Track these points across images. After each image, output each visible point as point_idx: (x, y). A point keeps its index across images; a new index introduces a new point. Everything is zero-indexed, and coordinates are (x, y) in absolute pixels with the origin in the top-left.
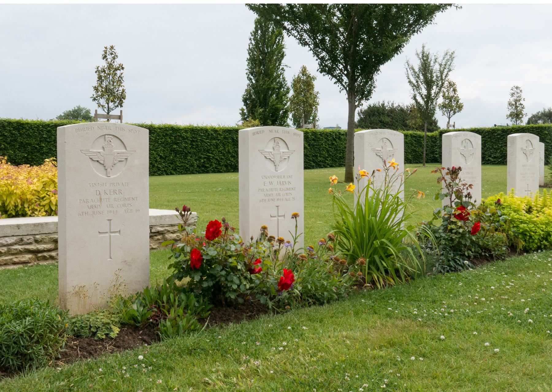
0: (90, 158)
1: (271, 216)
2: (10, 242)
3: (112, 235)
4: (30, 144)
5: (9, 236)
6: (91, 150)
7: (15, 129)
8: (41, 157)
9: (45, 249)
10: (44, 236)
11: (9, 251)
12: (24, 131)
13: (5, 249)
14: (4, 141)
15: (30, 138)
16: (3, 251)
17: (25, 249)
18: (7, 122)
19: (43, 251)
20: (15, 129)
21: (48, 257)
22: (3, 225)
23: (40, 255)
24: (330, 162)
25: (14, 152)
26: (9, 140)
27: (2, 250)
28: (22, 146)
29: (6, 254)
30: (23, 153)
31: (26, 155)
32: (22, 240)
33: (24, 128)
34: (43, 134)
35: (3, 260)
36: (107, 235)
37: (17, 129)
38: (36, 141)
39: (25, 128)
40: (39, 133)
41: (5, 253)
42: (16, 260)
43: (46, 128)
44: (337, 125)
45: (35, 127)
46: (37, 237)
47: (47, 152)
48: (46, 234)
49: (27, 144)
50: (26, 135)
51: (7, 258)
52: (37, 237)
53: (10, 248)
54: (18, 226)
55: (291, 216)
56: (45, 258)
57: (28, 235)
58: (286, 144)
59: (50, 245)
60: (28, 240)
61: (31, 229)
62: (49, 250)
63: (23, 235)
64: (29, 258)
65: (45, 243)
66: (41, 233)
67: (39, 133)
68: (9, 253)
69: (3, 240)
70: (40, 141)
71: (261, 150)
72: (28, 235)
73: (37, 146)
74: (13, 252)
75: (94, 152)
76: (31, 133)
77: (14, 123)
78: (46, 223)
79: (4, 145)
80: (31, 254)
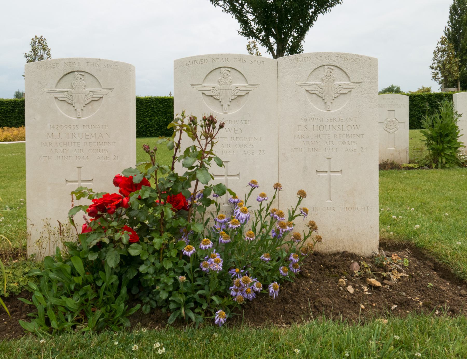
0: (306, 91)
3: (229, 178)
6: (203, 85)
24: (149, 135)
36: (326, 174)
44: (430, 87)
75: (60, 92)
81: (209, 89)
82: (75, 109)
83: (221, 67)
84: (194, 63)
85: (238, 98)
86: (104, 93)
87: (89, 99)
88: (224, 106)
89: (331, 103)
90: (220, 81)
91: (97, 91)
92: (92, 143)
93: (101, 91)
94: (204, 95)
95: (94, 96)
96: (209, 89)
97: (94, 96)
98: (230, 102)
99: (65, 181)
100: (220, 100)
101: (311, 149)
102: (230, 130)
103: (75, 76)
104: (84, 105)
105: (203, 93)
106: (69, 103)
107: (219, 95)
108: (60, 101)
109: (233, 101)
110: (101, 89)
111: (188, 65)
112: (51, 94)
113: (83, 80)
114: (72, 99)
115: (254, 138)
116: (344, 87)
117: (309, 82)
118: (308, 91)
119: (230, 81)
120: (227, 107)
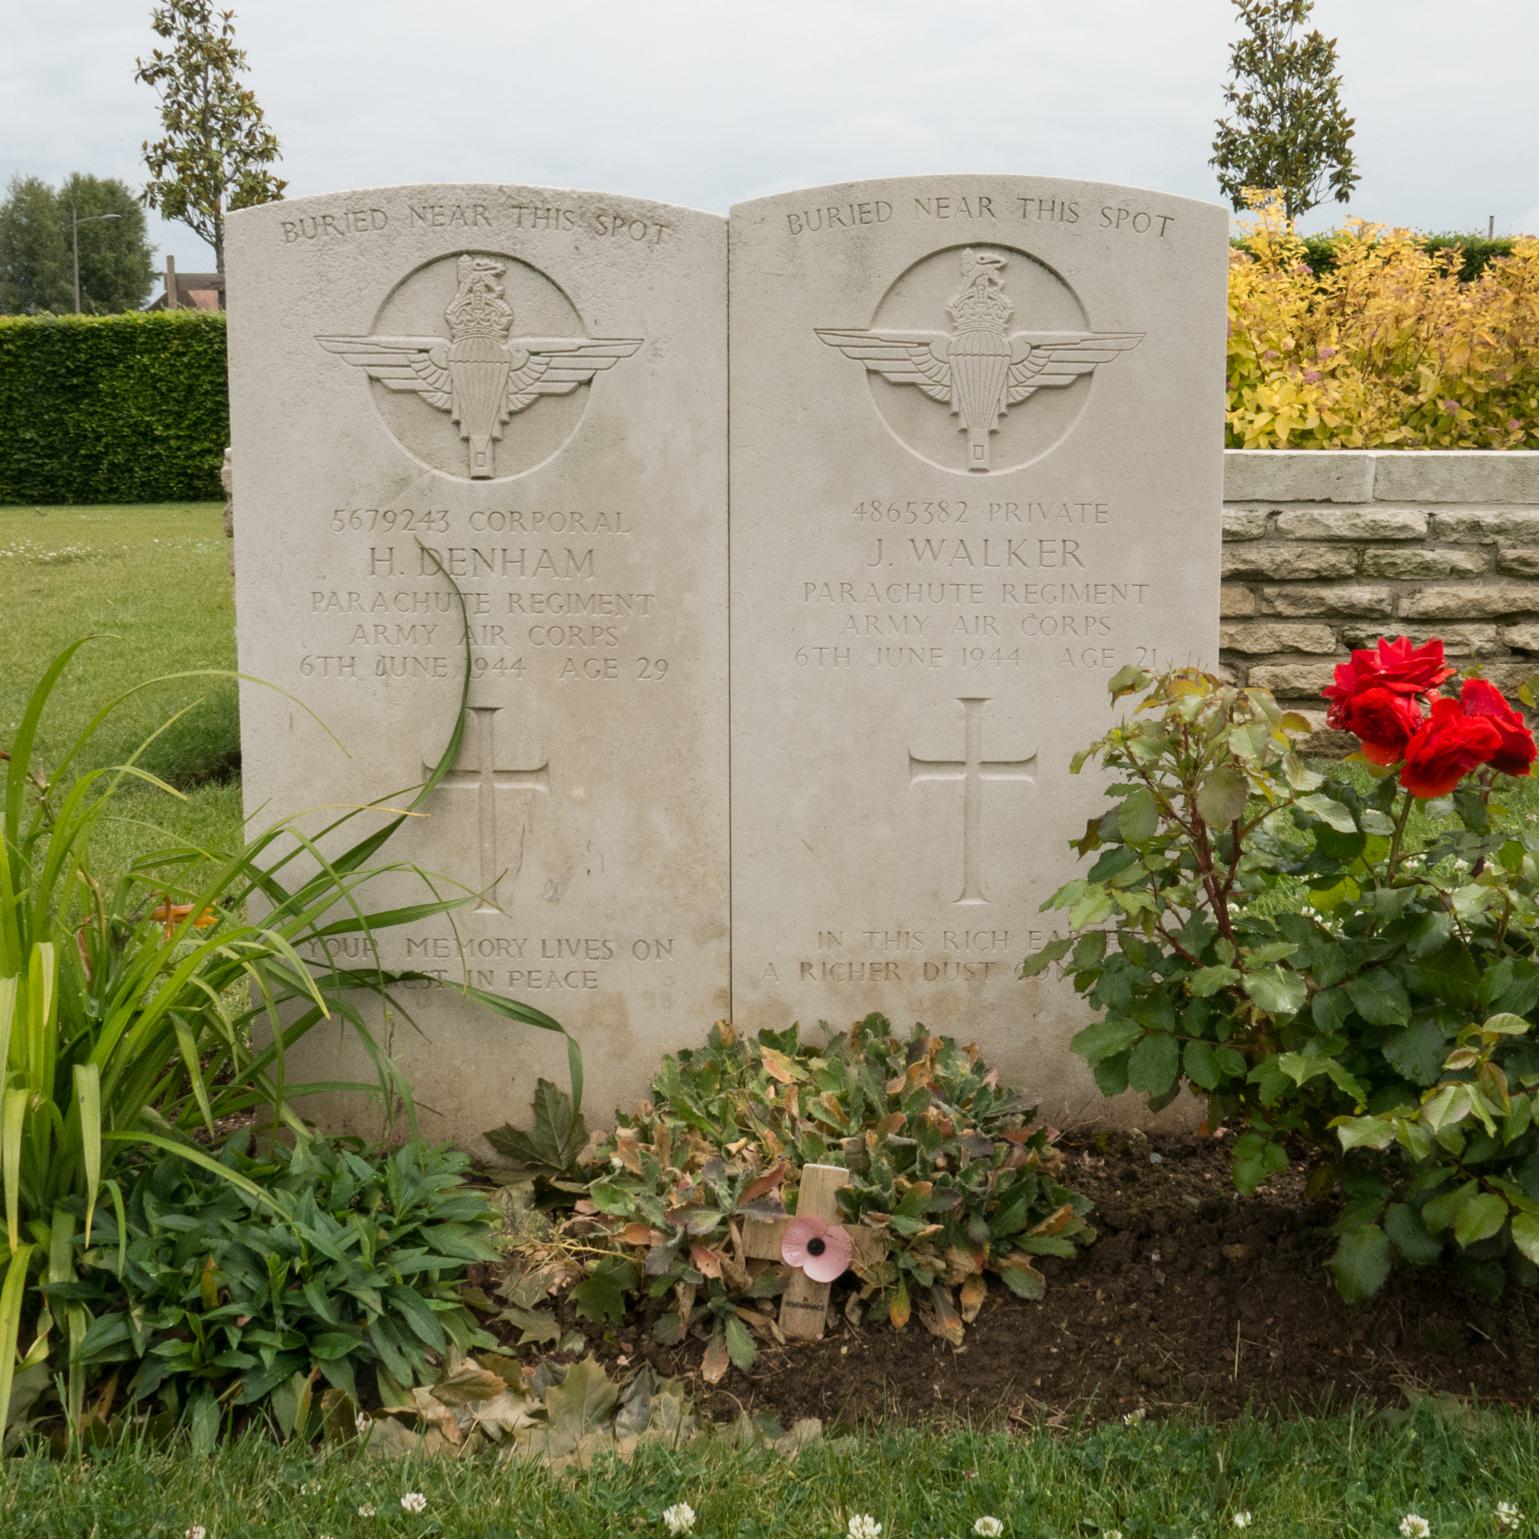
36: (958, 776)
81: (901, 353)
82: (464, 433)
83: (457, 255)
84: (825, 222)
87: (530, 389)
90: (955, 313)
91: (1065, 345)
92: (1039, 588)
95: (550, 374)
96: (901, 353)
97: (550, 374)
98: (504, 423)
99: (907, 761)
100: (955, 408)
102: (936, 549)
103: (967, 267)
104: (505, 417)
105: (373, 380)
107: (946, 381)
108: (886, 387)
110: (1086, 334)
111: (796, 227)
112: (848, 350)
113: (501, 297)
114: (447, 388)
116: (1056, 355)
117: (384, 339)
118: (378, 380)
119: (504, 320)
120: (985, 440)
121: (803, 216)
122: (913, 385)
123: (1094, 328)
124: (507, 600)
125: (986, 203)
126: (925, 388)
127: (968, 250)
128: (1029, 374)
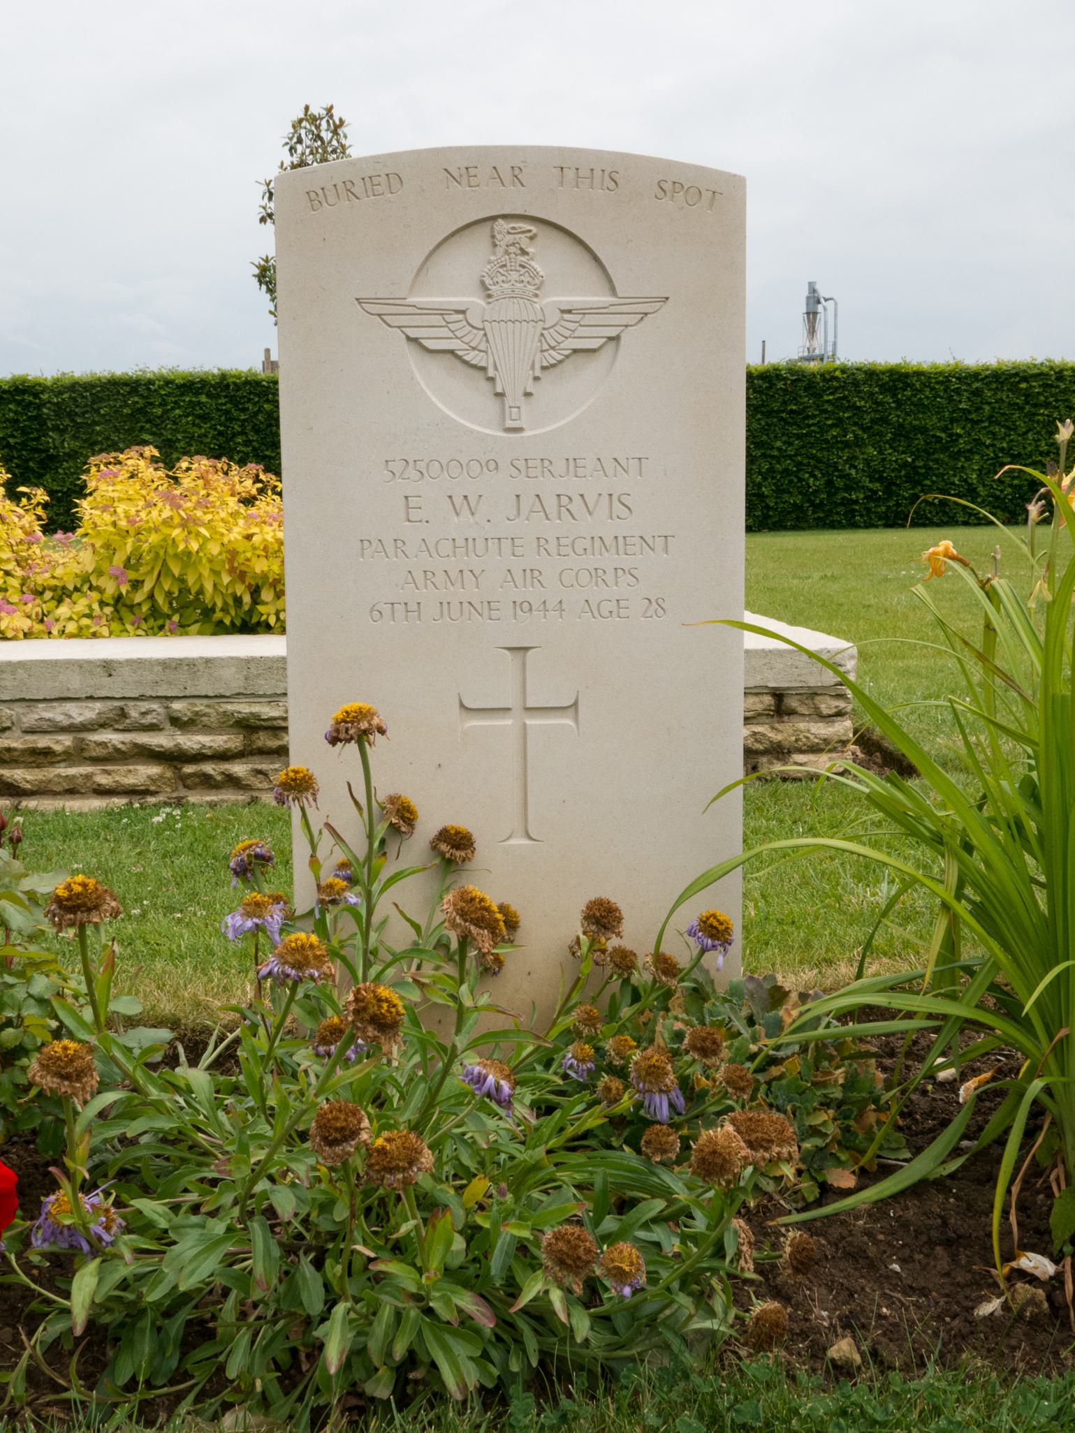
0: (409, 339)
1: (462, 706)
2: (78, 719)
3: (532, 722)
4: (923, 430)
5: (78, 699)
7: (884, 388)
8: (952, 463)
9: (208, 752)
10: (200, 706)
11: (82, 750)
12: (908, 393)
13: (66, 741)
14: (856, 424)
15: (924, 413)
16: (58, 748)
17: (136, 745)
18: (865, 372)
19: (199, 757)
20: (884, 388)
21: (219, 778)
22: (56, 661)
23: (189, 769)
25: (880, 452)
26: (867, 418)
27: (58, 742)
28: (901, 435)
29: (69, 757)
30: (904, 452)
31: (910, 460)
32: (123, 714)
33: (908, 385)
34: (960, 402)
35: (59, 776)
36: (507, 722)
37: (889, 390)
38: (940, 420)
39: (911, 386)
40: (950, 399)
41: (65, 752)
42: (103, 780)
43: (969, 385)
45: (938, 383)
46: (177, 706)
47: (970, 451)
48: (206, 697)
49: (914, 427)
50: (913, 404)
51: (72, 771)
52: (177, 706)
53: (83, 740)
54: (108, 667)
55: (327, 726)
56: (207, 782)
57: (141, 698)
58: (596, 259)
59: (225, 738)
60: (144, 714)
61: (150, 677)
62: (223, 756)
63: (124, 698)
64: (149, 777)
65: (207, 729)
66: (187, 694)
67: (950, 399)
68: (77, 754)
69: (59, 710)
70: (952, 421)
71: (370, 301)
72: (141, 698)
73: (943, 435)
74: (94, 754)
76: (927, 398)
77: (883, 373)
78: (208, 661)
79: (853, 432)
80: (160, 764)
81: (436, 320)
83: (494, 218)
85: (574, 357)
86: (624, 320)
88: (509, 401)
89: (528, 395)
93: (613, 309)
94: (413, 346)
98: (536, 379)
100: (491, 373)
101: (455, 606)
104: (538, 373)
106: (466, 363)
107: (482, 347)
109: (547, 372)
115: (637, 541)
121: (320, 192)
122: (452, 352)
123: (620, 293)
124: (535, 545)
125: (516, 175)
126: (460, 353)
127: (500, 221)
128: (560, 339)
